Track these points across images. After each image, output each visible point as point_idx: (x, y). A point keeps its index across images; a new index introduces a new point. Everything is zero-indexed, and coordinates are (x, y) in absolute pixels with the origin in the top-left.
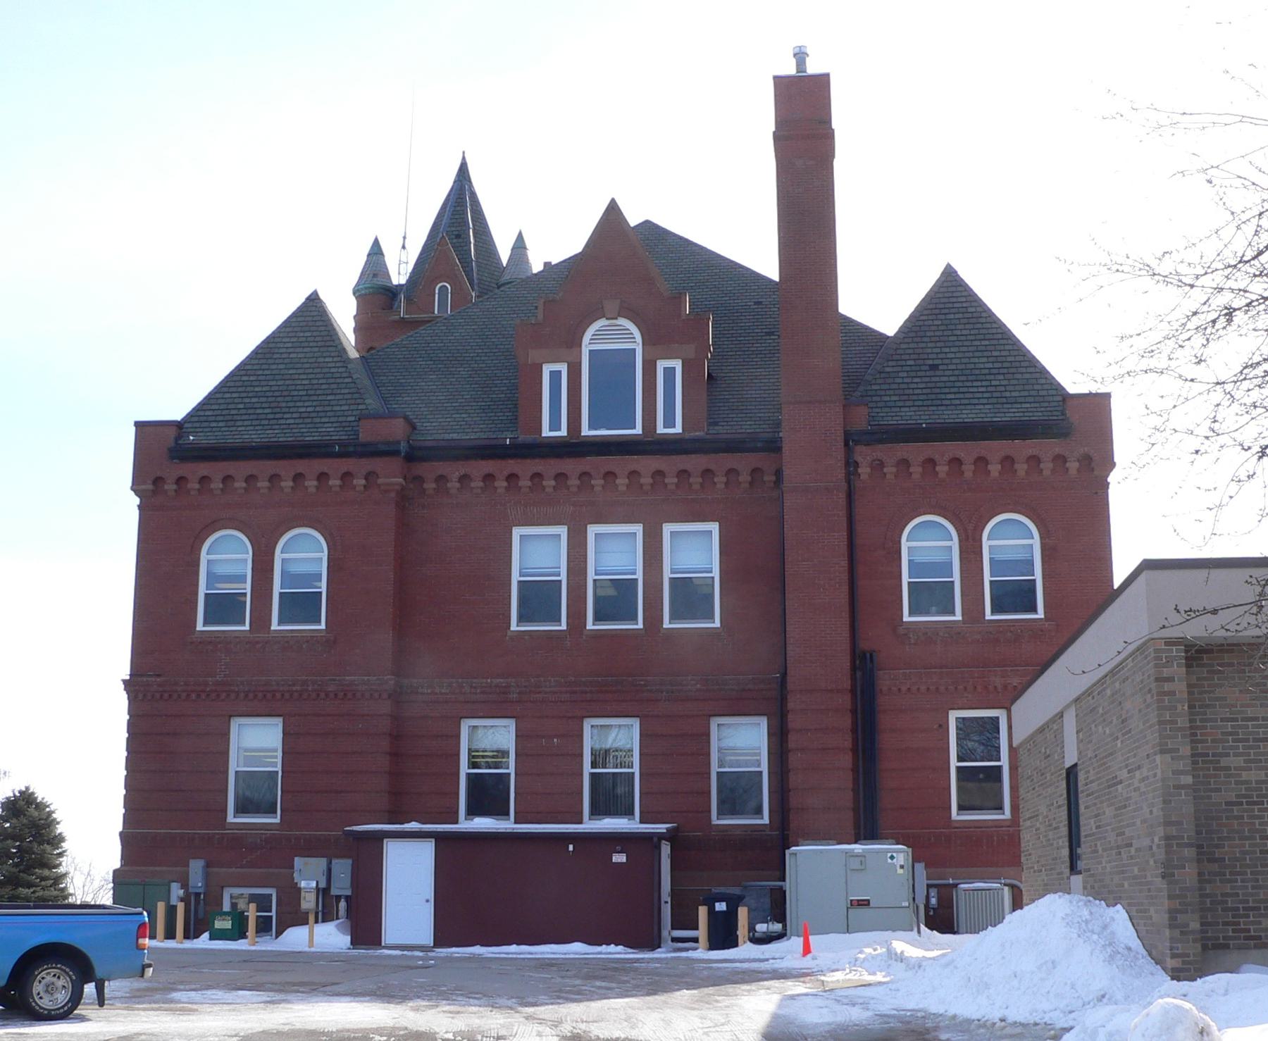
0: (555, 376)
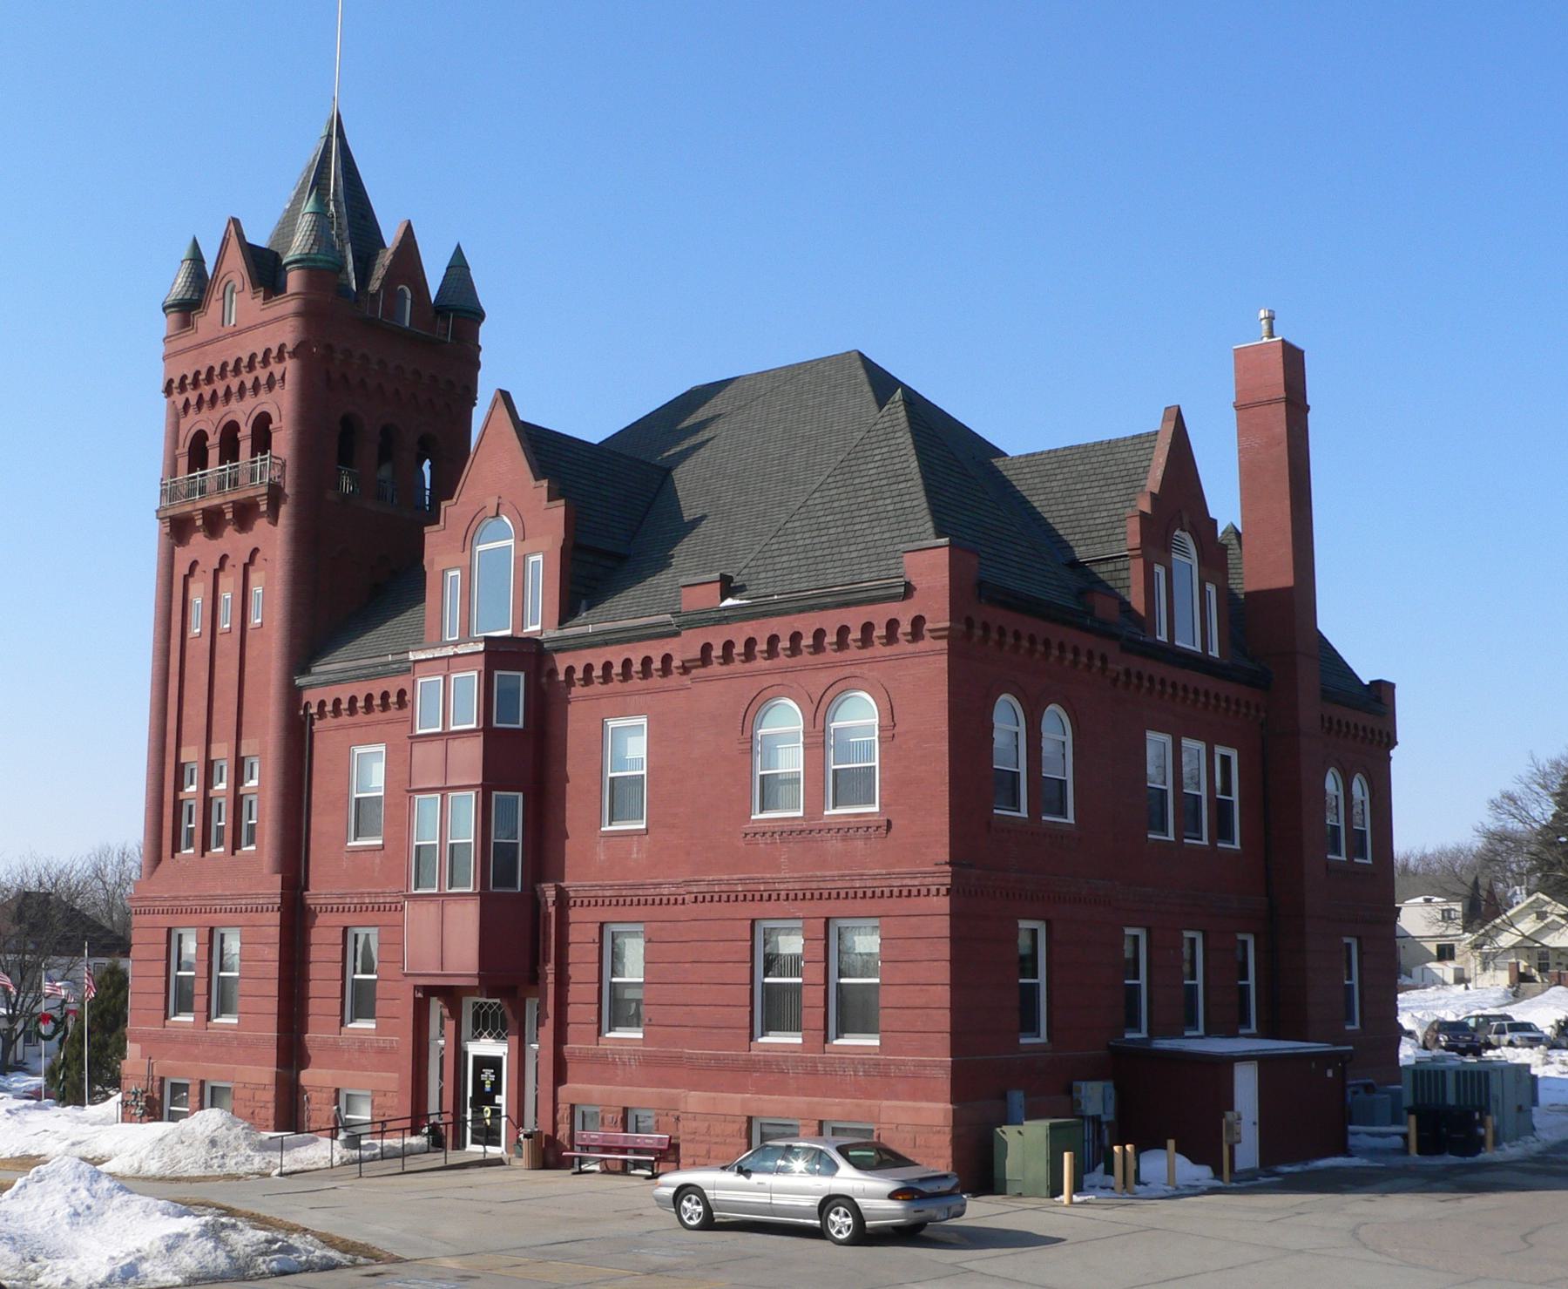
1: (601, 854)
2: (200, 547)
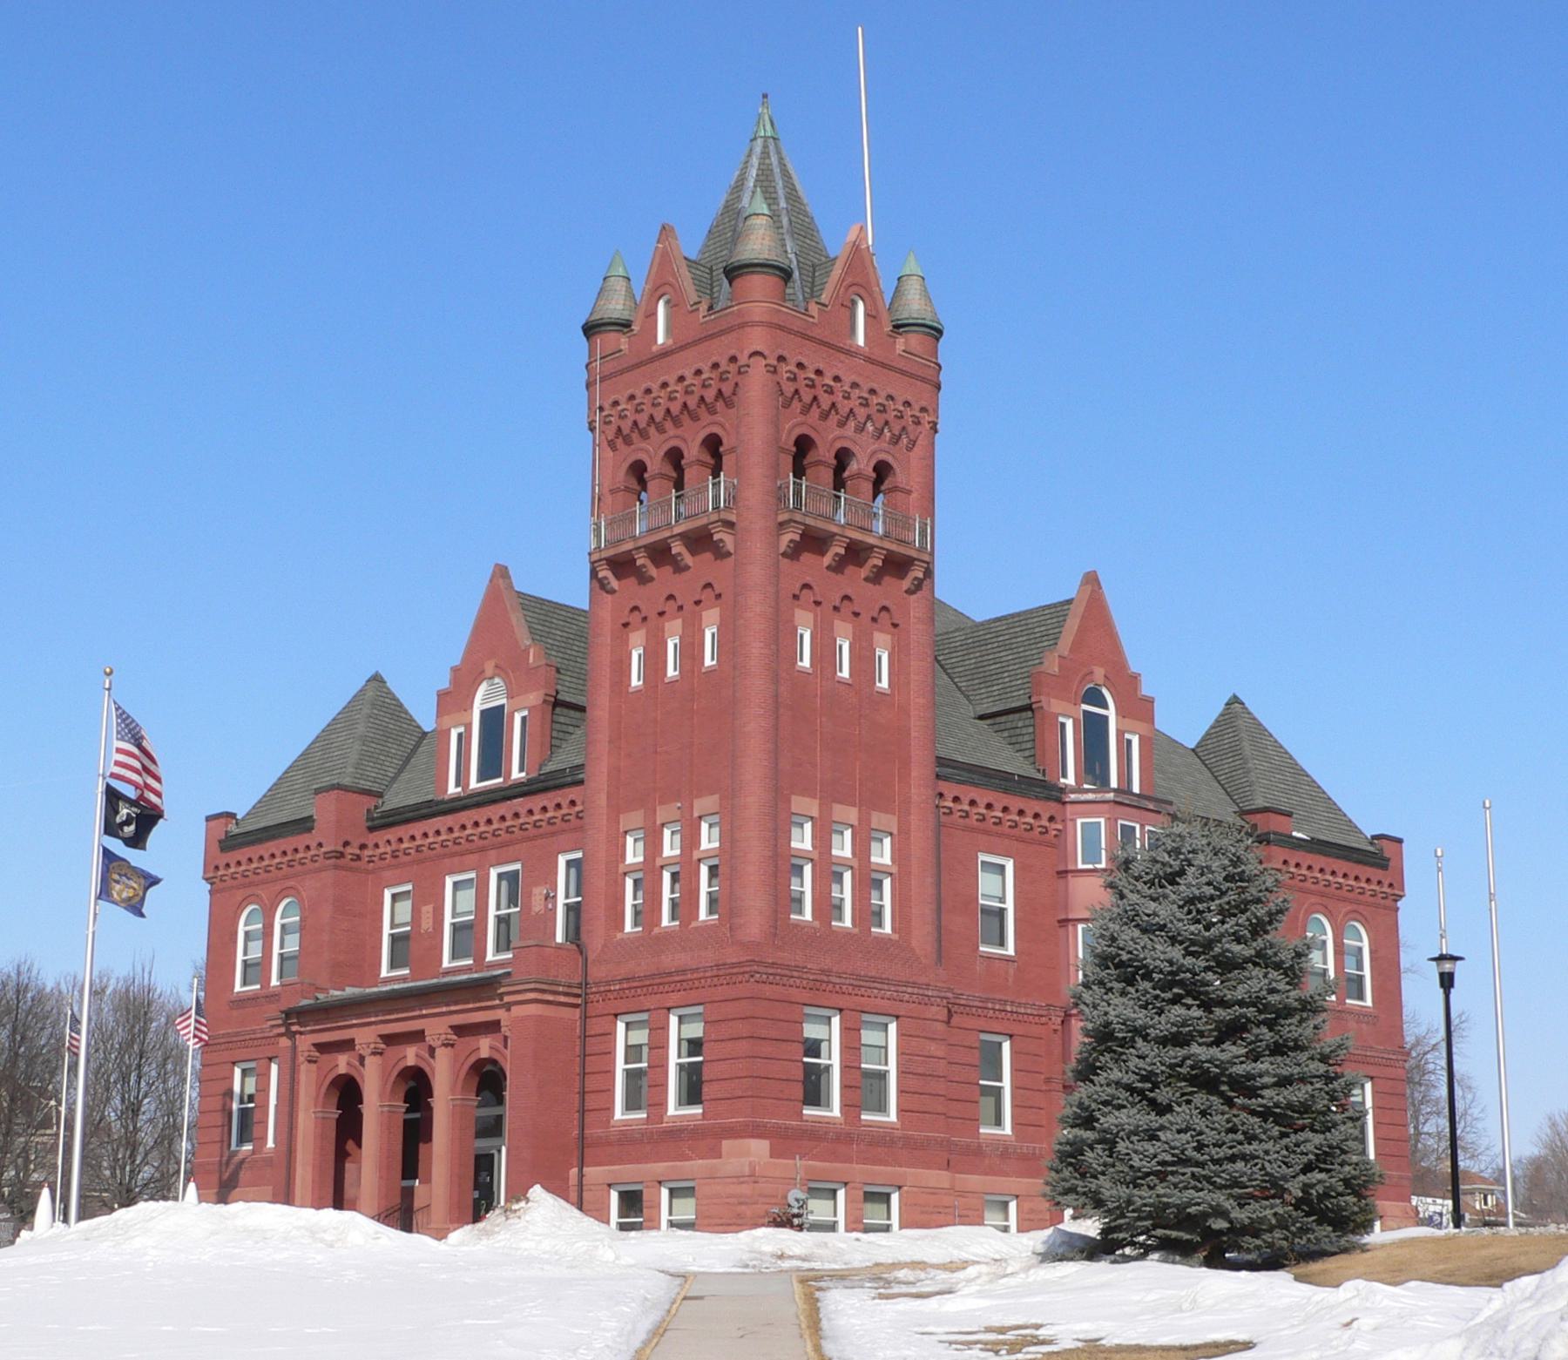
0: (1063, 725)
1: (979, 967)
2: (814, 566)
